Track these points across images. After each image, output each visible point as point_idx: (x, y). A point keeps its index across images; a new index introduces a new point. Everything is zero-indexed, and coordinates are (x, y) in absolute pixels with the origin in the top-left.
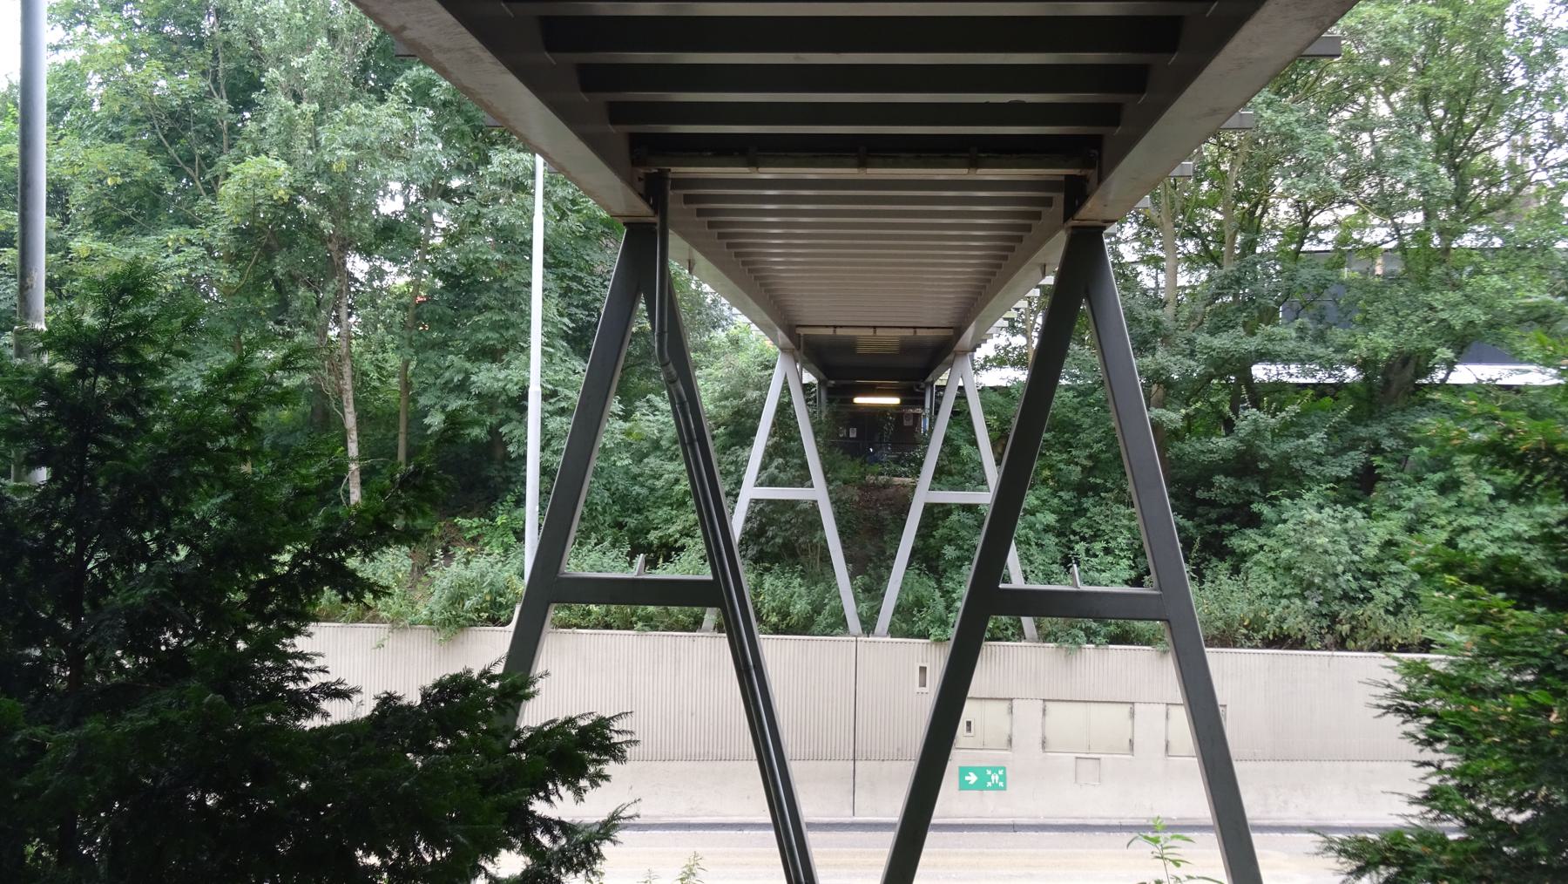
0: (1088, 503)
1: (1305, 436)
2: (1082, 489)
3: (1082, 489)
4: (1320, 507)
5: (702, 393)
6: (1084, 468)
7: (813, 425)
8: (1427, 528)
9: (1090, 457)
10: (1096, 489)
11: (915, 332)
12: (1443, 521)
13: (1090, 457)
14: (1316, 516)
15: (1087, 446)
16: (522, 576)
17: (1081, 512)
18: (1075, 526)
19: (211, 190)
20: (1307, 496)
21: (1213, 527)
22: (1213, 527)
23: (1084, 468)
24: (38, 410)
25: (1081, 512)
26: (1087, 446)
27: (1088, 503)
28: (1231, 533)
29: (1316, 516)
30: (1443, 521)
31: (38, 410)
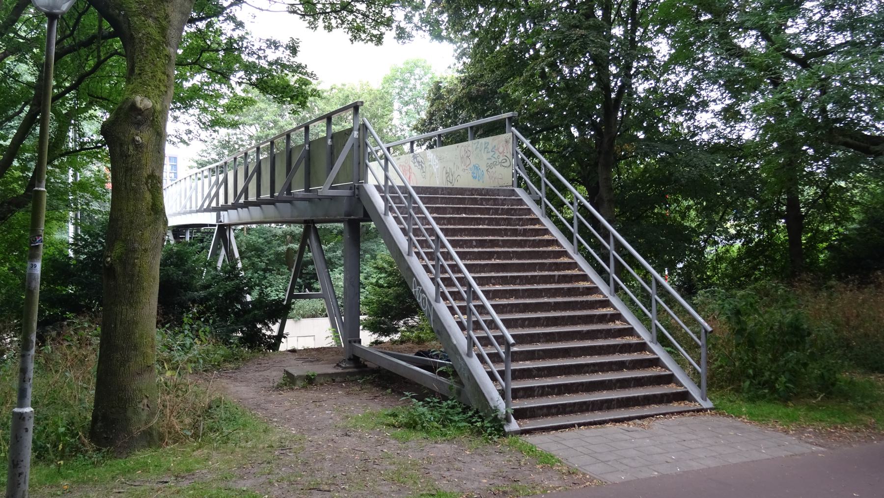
0: (267, 275)
1: (335, 252)
2: (265, 270)
3: (265, 270)
4: (340, 274)
5: (695, 465)
6: (266, 263)
7: (521, 378)
8: (370, 278)
9: (268, 260)
10: (270, 271)
11: (218, 217)
12: (375, 276)
13: (268, 260)
14: (339, 276)
15: (267, 256)
16: (146, 424)
17: (265, 278)
18: (263, 283)
19: (741, 400)
20: (336, 270)
21: (308, 281)
22: (308, 281)
23: (266, 263)
24: (584, 10)
25: (265, 278)
26: (267, 256)
27: (267, 275)
28: (314, 283)
29: (339, 276)
30: (375, 276)
31: (584, 10)
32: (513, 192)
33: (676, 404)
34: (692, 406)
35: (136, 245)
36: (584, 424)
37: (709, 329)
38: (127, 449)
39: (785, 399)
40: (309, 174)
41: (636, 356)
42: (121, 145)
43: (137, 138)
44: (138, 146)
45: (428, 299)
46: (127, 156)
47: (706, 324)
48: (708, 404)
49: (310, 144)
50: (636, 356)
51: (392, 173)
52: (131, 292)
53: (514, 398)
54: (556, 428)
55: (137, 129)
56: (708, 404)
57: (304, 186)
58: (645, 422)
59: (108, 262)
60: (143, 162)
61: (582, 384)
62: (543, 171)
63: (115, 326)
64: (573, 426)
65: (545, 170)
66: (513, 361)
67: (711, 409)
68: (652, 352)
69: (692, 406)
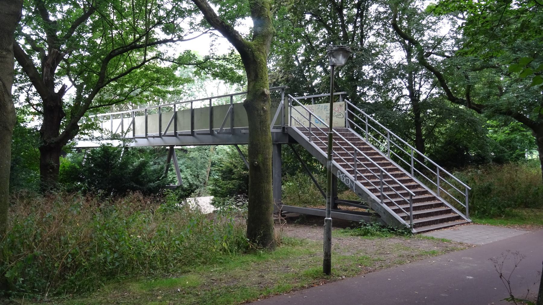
32: (347, 130)
33: (445, 223)
34: (463, 221)
35: (267, 156)
36: (461, 224)
37: (470, 189)
38: (272, 247)
39: (493, 216)
40: (233, 120)
41: (433, 202)
42: (257, 111)
43: (265, 108)
44: (265, 111)
45: (351, 180)
46: (261, 116)
47: (468, 187)
48: (469, 220)
49: (233, 105)
50: (433, 202)
51: (313, 121)
52: (267, 177)
53: (414, 218)
54: (452, 226)
55: (264, 103)
56: (469, 220)
57: (209, 127)
58: (454, 227)
59: (256, 164)
60: (267, 118)
61: (424, 214)
62: (367, 121)
63: (262, 193)
64: (432, 230)
65: (368, 120)
66: (413, 203)
67: (472, 222)
68: (439, 200)
69: (463, 221)
